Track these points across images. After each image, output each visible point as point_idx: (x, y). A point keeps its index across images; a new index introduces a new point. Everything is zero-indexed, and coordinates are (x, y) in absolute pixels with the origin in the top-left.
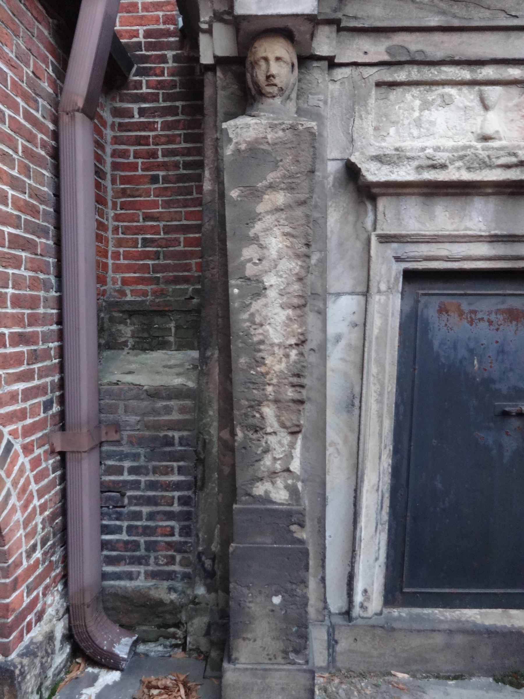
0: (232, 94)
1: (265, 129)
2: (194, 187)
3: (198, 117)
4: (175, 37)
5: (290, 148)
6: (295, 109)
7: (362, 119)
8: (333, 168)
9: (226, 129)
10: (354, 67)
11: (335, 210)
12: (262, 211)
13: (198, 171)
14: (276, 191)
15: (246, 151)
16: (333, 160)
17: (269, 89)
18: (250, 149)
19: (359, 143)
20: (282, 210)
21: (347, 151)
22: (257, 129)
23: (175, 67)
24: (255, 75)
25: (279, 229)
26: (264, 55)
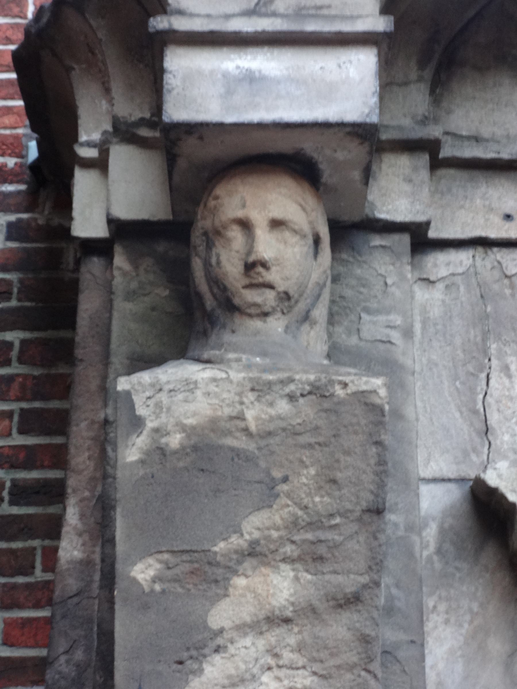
0: (153, 309)
1: (240, 394)
2: (39, 552)
3: (62, 369)
4: (18, 182)
5: (310, 446)
6: (325, 348)
7: (510, 376)
8: (436, 502)
9: (128, 394)
10: (480, 249)
11: (447, 622)
12: (227, 624)
13: (51, 510)
14: (267, 564)
15: (182, 452)
16: (435, 480)
17: (252, 296)
18: (195, 448)
19: (506, 438)
20: (287, 621)
21: (474, 457)
22: (216, 395)
23: (11, 250)
24: (214, 261)
25: (278, 679)
26: (240, 214)
